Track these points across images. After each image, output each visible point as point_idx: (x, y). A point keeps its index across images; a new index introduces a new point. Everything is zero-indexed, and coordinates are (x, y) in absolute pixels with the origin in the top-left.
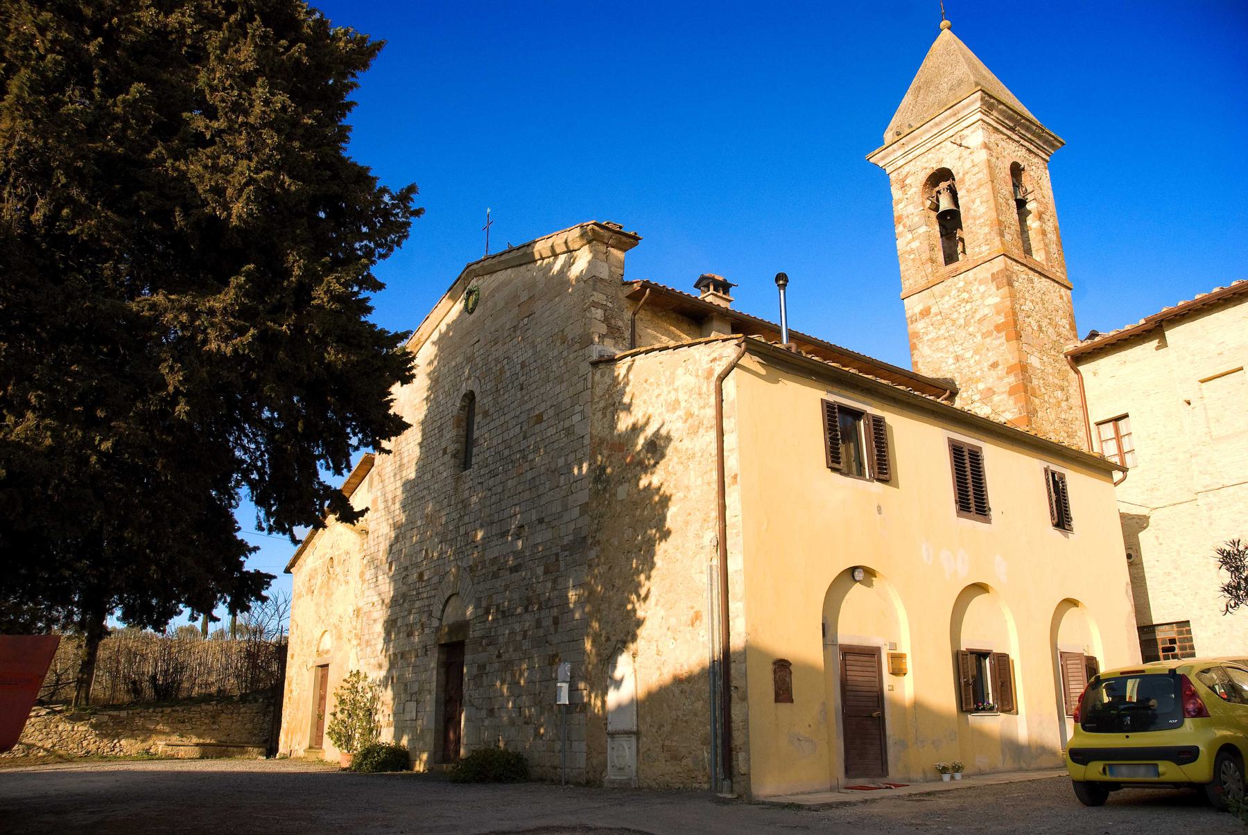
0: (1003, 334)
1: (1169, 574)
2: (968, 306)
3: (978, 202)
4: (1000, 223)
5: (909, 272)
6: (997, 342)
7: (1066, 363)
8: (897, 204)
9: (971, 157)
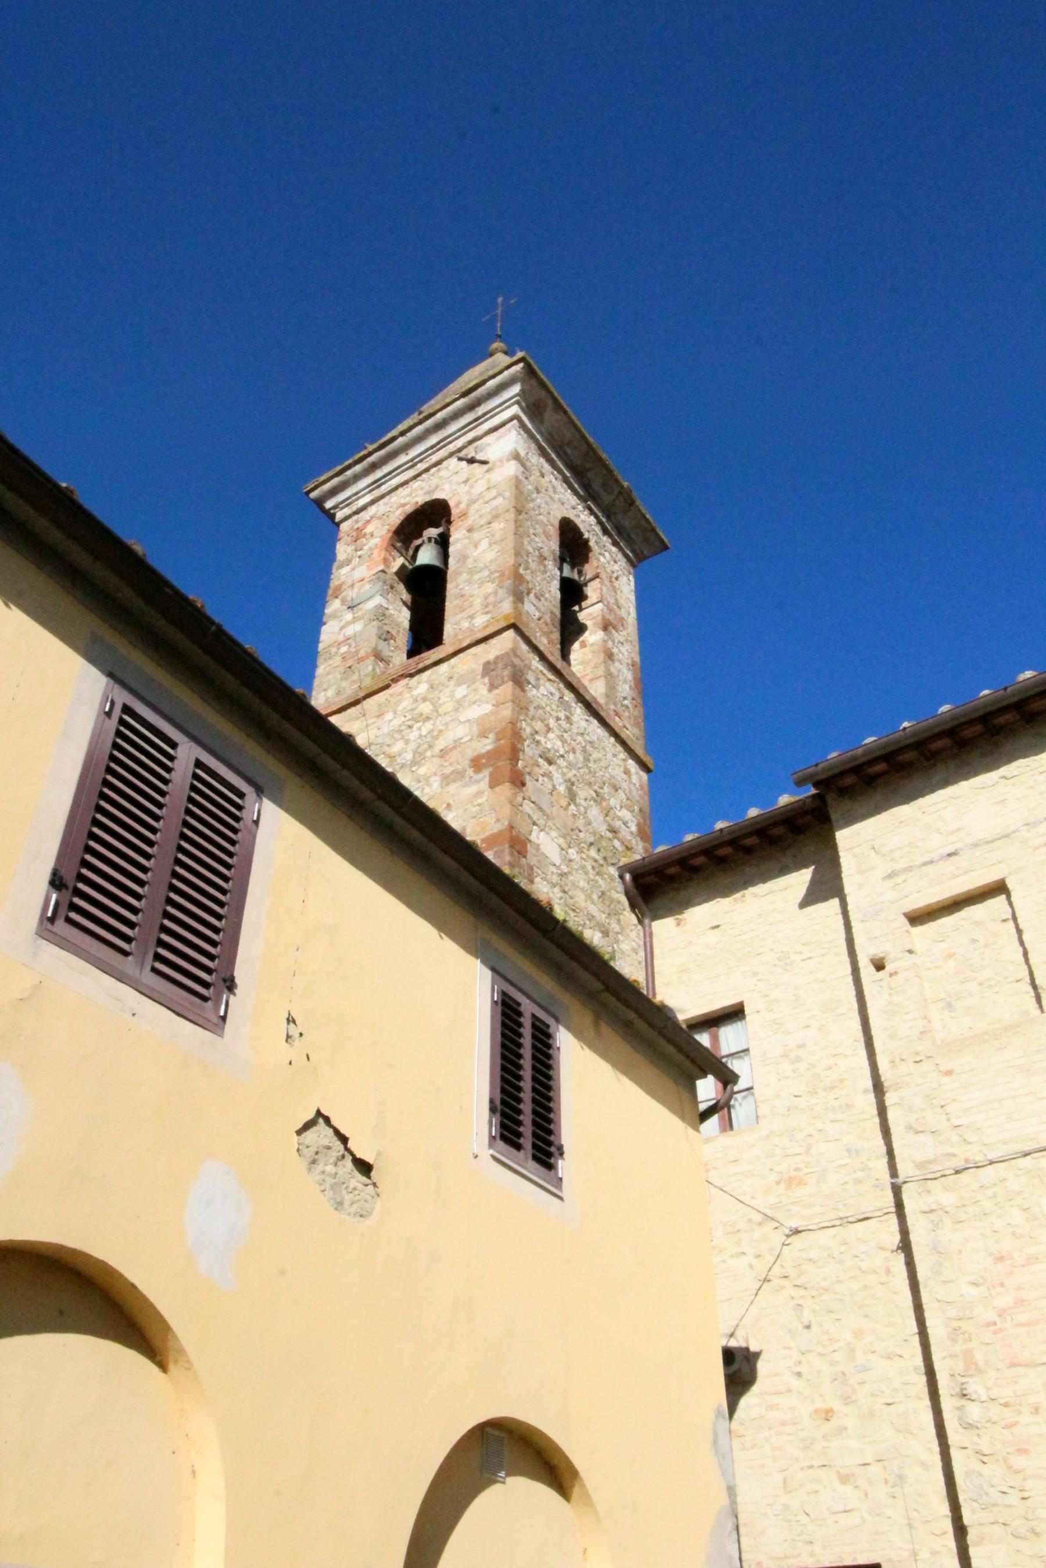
0: (486, 773)
1: (827, 1415)
2: (428, 726)
3: (485, 543)
4: (518, 578)
5: (330, 677)
6: (474, 789)
7: (620, 888)
8: (341, 567)
9: (488, 476)
